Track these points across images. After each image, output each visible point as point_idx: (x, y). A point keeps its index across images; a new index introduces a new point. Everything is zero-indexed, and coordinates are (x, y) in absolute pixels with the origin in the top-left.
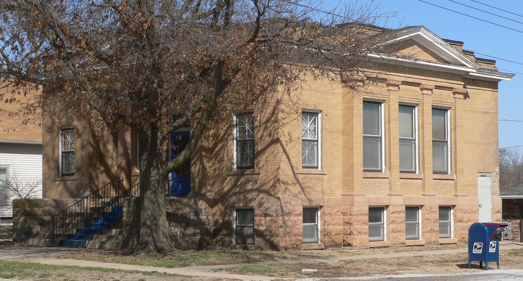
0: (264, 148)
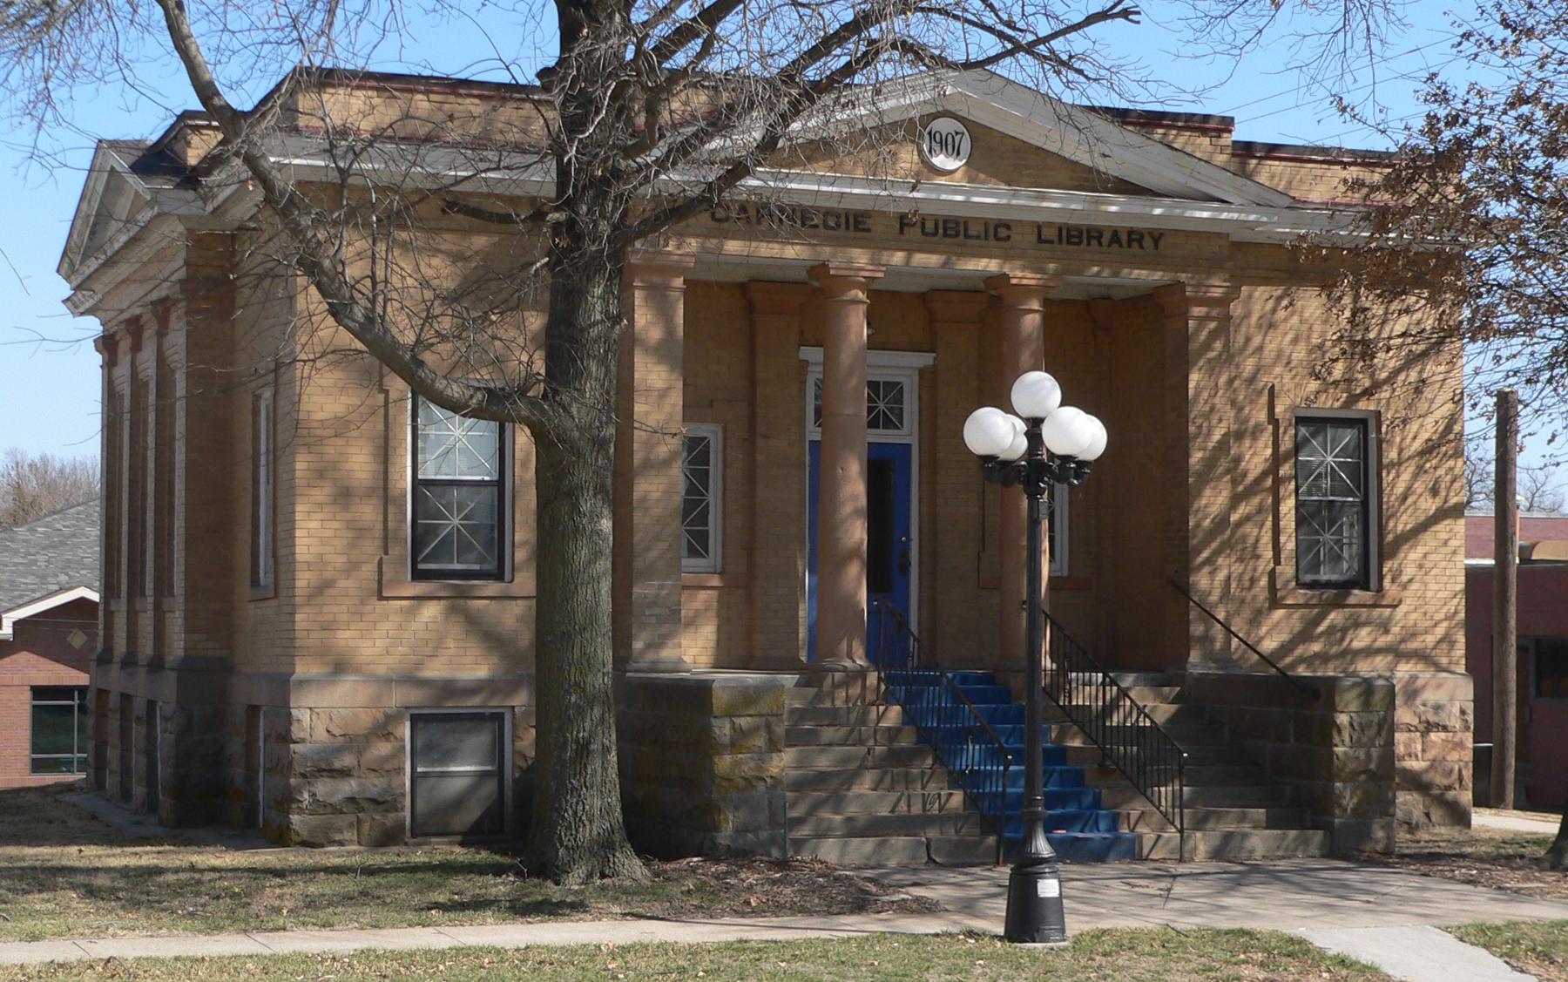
0: (1411, 530)
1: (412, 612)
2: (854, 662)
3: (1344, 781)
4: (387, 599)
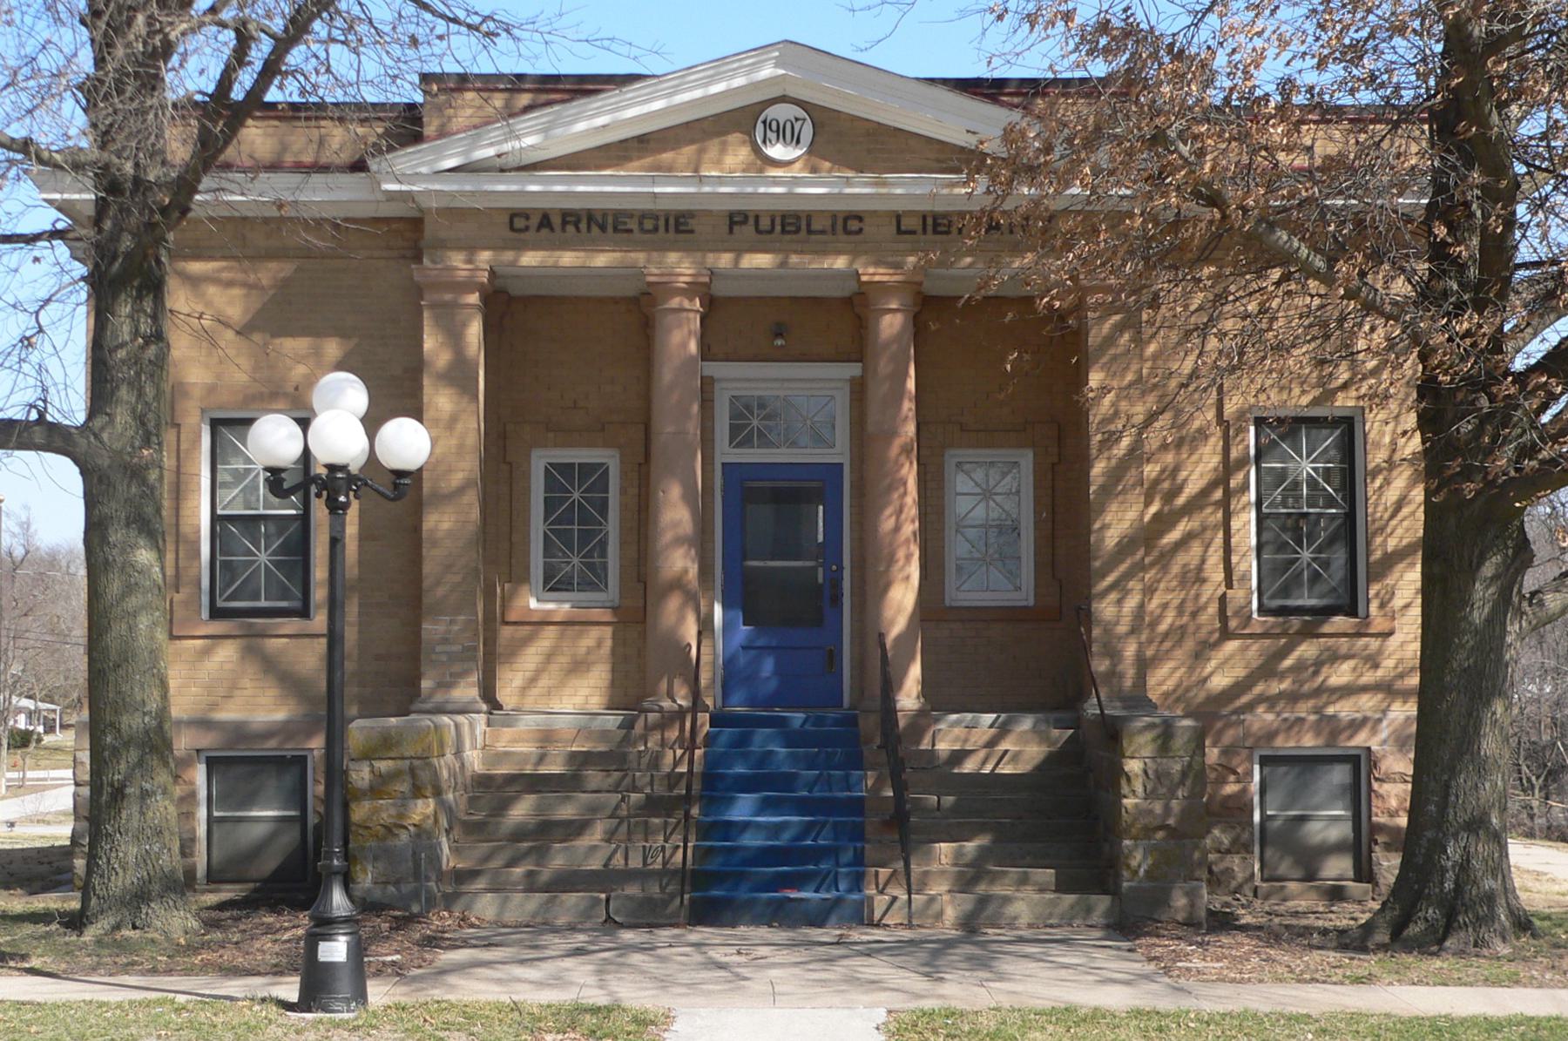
1: (206, 652)
2: (674, 701)
3: (1135, 838)
4: (180, 638)
